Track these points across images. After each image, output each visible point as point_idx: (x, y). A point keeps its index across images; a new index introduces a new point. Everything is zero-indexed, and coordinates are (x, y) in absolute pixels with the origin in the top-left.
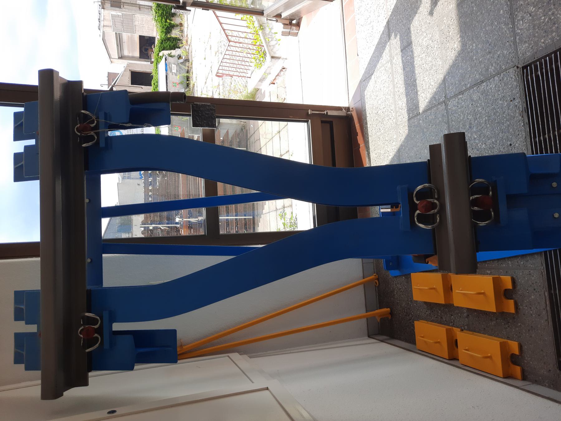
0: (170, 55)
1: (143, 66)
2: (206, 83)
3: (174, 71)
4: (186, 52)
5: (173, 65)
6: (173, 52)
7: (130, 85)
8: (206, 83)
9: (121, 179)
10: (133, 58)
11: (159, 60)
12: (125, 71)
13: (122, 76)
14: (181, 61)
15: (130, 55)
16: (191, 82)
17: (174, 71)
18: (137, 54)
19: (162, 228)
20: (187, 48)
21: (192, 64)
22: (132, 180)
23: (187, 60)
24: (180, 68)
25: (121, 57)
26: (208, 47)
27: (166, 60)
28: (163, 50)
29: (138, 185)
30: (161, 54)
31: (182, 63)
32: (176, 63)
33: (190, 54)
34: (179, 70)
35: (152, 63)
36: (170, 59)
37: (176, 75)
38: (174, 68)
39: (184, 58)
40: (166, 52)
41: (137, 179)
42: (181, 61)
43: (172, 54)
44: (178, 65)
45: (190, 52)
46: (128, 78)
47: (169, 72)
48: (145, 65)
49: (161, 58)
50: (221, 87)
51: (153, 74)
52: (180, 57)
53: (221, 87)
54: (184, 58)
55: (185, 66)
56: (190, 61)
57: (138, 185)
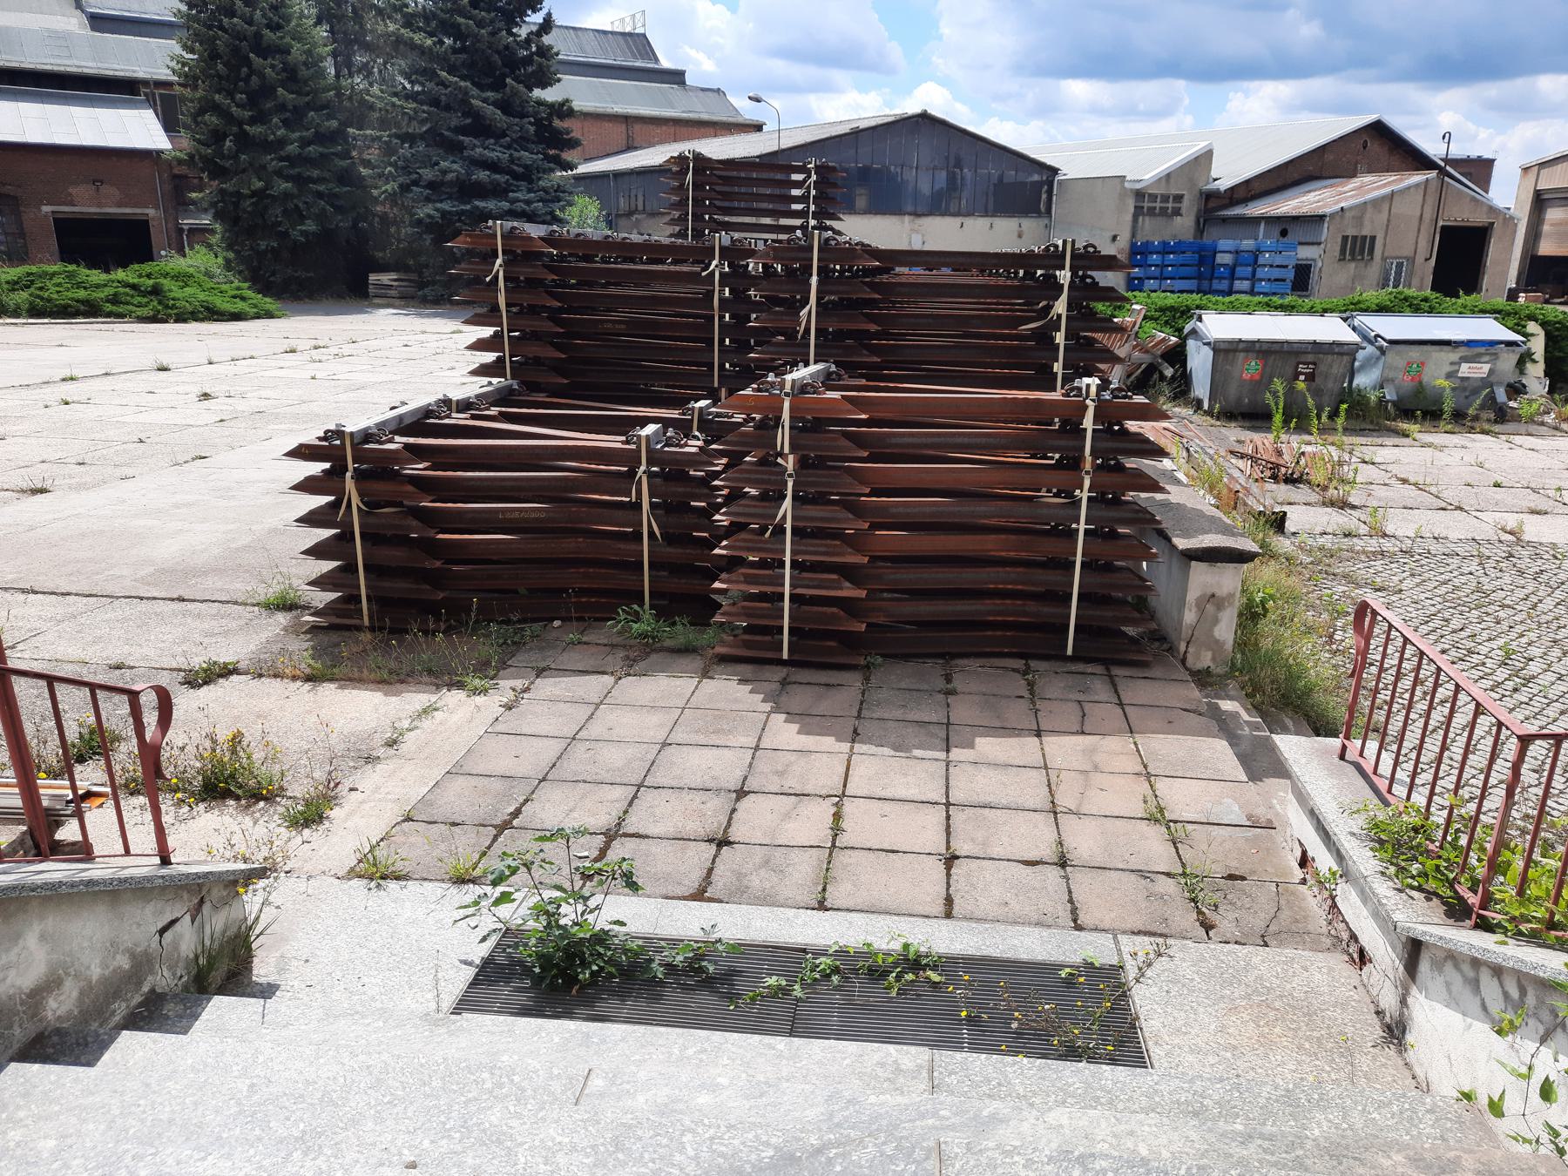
0: (1525, 358)
1: (1504, 264)
2: (1405, 481)
3: (1465, 370)
4: (1532, 415)
5: (1486, 368)
6: (1536, 370)
7: (1441, 223)
8: (1405, 481)
9: (1138, 186)
10: (1534, 234)
11: (1511, 321)
12: (1492, 210)
13: (1476, 201)
14: (1501, 395)
15: (1546, 228)
16: (1417, 427)
17: (1465, 370)
18: (1546, 248)
19: (804, 312)
20: (1550, 419)
21: (1483, 432)
22: (1129, 217)
23: (1502, 416)
24: (1475, 392)
25: (1540, 201)
26: (1542, 504)
27: (1510, 344)
28: (1548, 336)
29: (1114, 238)
30: (1532, 327)
31: (1492, 397)
32: (1493, 379)
33: (1522, 427)
34: (1467, 388)
35: (1512, 295)
36: (1508, 361)
37: (1449, 376)
38: (1480, 370)
39: (1512, 404)
40: (1538, 345)
41: (1133, 235)
42: (1501, 395)
43: (1529, 365)
44: (1487, 383)
45: (1533, 428)
46: (1465, 217)
47: (1463, 351)
48: (1506, 273)
49: (1518, 328)
50: (1373, 544)
51: (1465, 299)
52: (1516, 390)
53: (1373, 544)
54: (1512, 404)
55: (1482, 407)
56: (1497, 428)
57: (1114, 238)
